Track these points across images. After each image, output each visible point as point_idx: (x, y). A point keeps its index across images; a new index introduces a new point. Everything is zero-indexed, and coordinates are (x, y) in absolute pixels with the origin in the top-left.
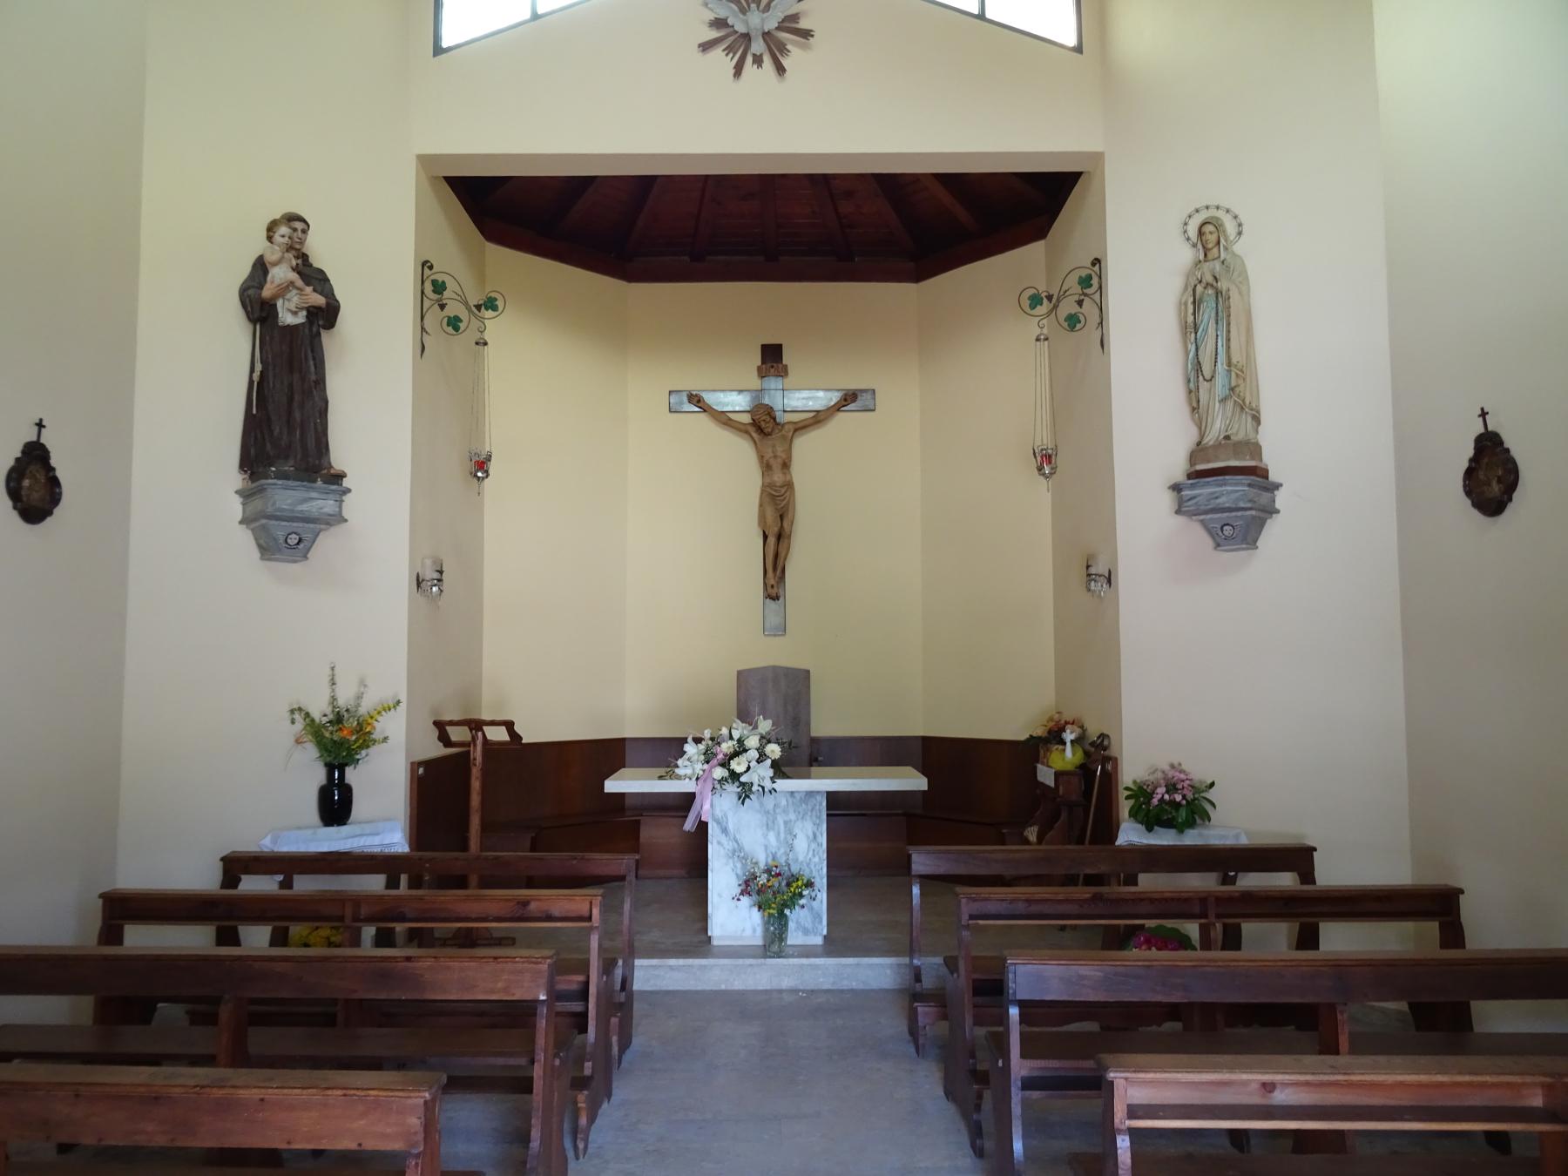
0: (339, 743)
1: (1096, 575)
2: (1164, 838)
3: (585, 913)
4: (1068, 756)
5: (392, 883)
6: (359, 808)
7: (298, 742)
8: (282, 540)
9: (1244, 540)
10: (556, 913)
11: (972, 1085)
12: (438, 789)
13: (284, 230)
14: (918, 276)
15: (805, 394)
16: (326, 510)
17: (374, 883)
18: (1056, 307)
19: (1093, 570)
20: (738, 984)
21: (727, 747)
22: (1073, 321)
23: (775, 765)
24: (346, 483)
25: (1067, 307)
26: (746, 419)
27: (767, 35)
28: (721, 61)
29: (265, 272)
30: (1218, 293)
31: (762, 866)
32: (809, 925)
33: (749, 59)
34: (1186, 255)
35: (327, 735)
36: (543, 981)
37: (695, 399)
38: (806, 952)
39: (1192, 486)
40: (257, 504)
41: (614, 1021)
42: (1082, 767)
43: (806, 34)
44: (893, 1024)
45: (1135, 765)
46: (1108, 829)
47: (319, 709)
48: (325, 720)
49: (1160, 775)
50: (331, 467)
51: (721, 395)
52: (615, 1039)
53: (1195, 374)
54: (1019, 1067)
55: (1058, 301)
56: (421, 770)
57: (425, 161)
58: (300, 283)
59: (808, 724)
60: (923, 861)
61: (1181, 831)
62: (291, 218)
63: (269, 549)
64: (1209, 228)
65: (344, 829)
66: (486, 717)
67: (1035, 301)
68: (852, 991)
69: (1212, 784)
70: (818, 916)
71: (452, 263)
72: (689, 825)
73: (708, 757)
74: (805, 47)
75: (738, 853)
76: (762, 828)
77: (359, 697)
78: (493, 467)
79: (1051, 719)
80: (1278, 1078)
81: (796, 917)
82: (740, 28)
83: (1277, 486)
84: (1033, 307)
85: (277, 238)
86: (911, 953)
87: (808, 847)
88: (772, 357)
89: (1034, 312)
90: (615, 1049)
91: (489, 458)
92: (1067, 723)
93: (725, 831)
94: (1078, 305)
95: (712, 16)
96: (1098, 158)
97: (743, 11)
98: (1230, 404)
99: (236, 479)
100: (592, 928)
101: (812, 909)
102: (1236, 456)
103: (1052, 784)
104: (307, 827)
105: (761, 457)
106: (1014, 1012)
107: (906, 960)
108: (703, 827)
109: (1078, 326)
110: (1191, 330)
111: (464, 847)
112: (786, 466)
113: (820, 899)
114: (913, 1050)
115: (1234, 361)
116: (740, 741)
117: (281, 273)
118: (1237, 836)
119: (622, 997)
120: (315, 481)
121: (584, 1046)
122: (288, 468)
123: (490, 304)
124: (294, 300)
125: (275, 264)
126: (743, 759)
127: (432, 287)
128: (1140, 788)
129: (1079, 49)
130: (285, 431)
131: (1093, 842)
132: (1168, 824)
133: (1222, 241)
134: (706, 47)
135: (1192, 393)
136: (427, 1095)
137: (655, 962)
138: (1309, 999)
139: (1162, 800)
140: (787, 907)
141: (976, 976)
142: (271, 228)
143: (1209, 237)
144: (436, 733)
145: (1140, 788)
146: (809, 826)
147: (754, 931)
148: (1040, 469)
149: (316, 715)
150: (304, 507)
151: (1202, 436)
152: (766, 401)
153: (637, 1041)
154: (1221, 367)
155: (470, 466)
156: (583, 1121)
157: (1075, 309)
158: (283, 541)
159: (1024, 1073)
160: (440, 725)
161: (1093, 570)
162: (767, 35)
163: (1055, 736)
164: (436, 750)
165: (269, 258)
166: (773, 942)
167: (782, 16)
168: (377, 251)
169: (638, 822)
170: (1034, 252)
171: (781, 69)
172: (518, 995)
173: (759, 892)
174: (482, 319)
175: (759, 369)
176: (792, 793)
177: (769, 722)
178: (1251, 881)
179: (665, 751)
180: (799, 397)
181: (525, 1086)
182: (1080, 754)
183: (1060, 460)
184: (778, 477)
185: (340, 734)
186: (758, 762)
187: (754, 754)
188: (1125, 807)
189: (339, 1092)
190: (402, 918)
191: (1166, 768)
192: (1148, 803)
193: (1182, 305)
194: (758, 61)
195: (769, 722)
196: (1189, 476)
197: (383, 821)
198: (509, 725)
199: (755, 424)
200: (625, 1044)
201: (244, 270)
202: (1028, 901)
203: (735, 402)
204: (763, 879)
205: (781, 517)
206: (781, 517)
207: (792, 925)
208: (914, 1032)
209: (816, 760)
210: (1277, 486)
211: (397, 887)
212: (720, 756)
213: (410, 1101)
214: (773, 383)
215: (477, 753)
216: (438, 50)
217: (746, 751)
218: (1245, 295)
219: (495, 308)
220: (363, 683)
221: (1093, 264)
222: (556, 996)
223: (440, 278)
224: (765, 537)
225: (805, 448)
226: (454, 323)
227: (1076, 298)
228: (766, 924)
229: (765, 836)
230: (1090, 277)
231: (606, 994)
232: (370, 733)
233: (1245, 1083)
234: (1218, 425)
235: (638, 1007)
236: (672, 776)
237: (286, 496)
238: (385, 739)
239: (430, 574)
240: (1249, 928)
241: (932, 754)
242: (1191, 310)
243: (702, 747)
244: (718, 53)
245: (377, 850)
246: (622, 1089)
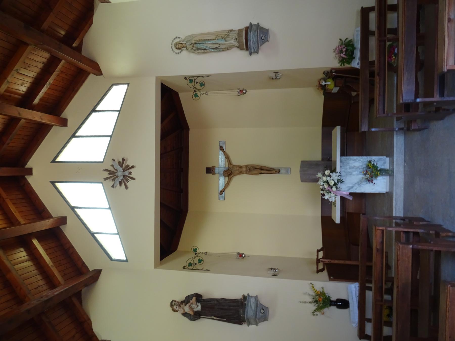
0: (323, 302)
1: (275, 77)
2: (357, 54)
3: (380, 232)
4: (330, 83)
5: (370, 289)
6: (344, 297)
7: (323, 314)
8: (263, 314)
9: (267, 33)
10: (381, 240)
11: (439, 112)
12: (337, 273)
13: (175, 307)
14: (188, 129)
15: (220, 161)
16: (254, 301)
17: (369, 295)
18: (198, 90)
19: (274, 77)
20: (402, 184)
21: (326, 186)
22: (202, 85)
23: (332, 172)
24: (246, 295)
25: (198, 86)
26: (227, 178)
27: (124, 170)
28: (130, 183)
29: (186, 313)
30: (195, 43)
31: (364, 176)
32: (383, 162)
33: (130, 175)
34: (185, 53)
35: (321, 305)
36: (406, 246)
37: (221, 193)
38: (392, 163)
39: (251, 49)
40: (252, 321)
41: (415, 223)
42: (333, 79)
43: (124, 160)
44: (417, 136)
45: (333, 63)
46: (354, 71)
47: (313, 307)
48: (316, 305)
49: (337, 56)
50: (241, 299)
51: (220, 185)
52: (421, 223)
53: (218, 49)
54: (437, 98)
55: (196, 89)
56: (332, 278)
57: (156, 266)
58: (189, 304)
59: (318, 161)
60: (364, 128)
61: (355, 48)
62: (172, 305)
63: (265, 318)
64: (177, 46)
65: (350, 302)
66: (316, 257)
67: (196, 95)
68: (405, 149)
69: (340, 39)
70: (380, 160)
71: (184, 260)
72: (350, 198)
73: (329, 192)
74: (127, 160)
75: (359, 183)
76: (352, 176)
77: (309, 295)
78: (241, 252)
79: (318, 89)
80: (447, 17)
81: (380, 166)
82: (122, 178)
83: (251, 24)
84: (198, 96)
85: (177, 309)
86: (392, 130)
87: (358, 162)
88: (210, 170)
89: (199, 95)
90: (424, 223)
91: (239, 253)
92: (319, 84)
93: (352, 187)
94: (197, 83)
95: (119, 185)
96: (157, 78)
97: (117, 177)
98: (227, 39)
99: (245, 326)
100: (386, 229)
101: (377, 161)
102: (242, 36)
103: (338, 88)
104: (350, 313)
105: (238, 174)
106: (418, 100)
107: (395, 133)
108: (351, 194)
109: (203, 83)
110: (205, 51)
111: (357, 266)
112: (241, 167)
113: (374, 158)
114: (426, 130)
115: (214, 38)
116: (324, 182)
117: (187, 309)
118: (357, 31)
119: (407, 220)
120: (245, 304)
121: (423, 233)
122: (242, 311)
123: (195, 250)
124: (194, 306)
125: (184, 310)
126: (330, 182)
127: (190, 266)
128: (341, 61)
129: (128, 84)
130: (231, 311)
131: (359, 75)
132: (353, 52)
133: (181, 42)
134: (126, 187)
135: (223, 50)
136: (449, 286)
137: (394, 209)
138: (416, 7)
139: (345, 55)
140: (377, 169)
141: (403, 111)
142: (174, 311)
143: (180, 46)
144: (320, 273)
145: (341, 61)
146: (351, 162)
147: (384, 179)
148: (244, 93)
149: (315, 308)
150: (253, 307)
151: (236, 46)
152: (222, 172)
153: (421, 215)
154: (216, 42)
155: (241, 258)
156: (450, 234)
157: (198, 84)
158: (262, 314)
159: (438, 96)
160: (318, 271)
161: (274, 77)
162: (124, 170)
163: (323, 88)
164: (325, 273)
165: (182, 312)
166: (388, 173)
167: (119, 166)
168: (180, 281)
169: (348, 213)
170: (182, 96)
171: (133, 167)
172: (410, 254)
173: (372, 177)
174: (199, 253)
175: (213, 174)
176: (341, 167)
177: (318, 173)
178: (373, 26)
179: (326, 205)
180: (221, 162)
181: (438, 253)
182: (329, 80)
183: (241, 88)
184: (244, 169)
185: (321, 301)
186: (331, 177)
187: (328, 178)
188: (347, 66)
189: (448, 314)
190: (382, 287)
191: (335, 53)
192: (346, 59)
193: (198, 54)
194: (130, 173)
195: (318, 173)
196: (247, 50)
197: (349, 290)
198: (318, 251)
199: (229, 175)
200: (423, 220)
201: (186, 319)
202: (379, 96)
203: (222, 181)
204: (368, 176)
205: (256, 168)
206: (256, 168)
207: (383, 167)
208: (419, 130)
209: (329, 159)
210: (251, 24)
211: (371, 287)
212: (329, 188)
213: (451, 292)
214: (217, 170)
215: (327, 261)
216: (126, 261)
217: (327, 181)
218: (196, 35)
219: (196, 249)
220: (305, 294)
221: (186, 79)
222: (407, 242)
223: (188, 264)
224: (261, 173)
225: (236, 161)
226: (200, 261)
227: (195, 84)
228: (382, 175)
229: (354, 175)
230: (190, 80)
231: (406, 226)
232: (320, 292)
233: (448, 27)
234: (232, 42)
235: (409, 215)
236: (335, 203)
237: (250, 312)
238: (322, 288)
239: (272, 272)
240: (389, 26)
241: (328, 123)
242: (199, 51)
243: (326, 194)
244: (128, 184)
245: (358, 293)
246: (438, 221)
